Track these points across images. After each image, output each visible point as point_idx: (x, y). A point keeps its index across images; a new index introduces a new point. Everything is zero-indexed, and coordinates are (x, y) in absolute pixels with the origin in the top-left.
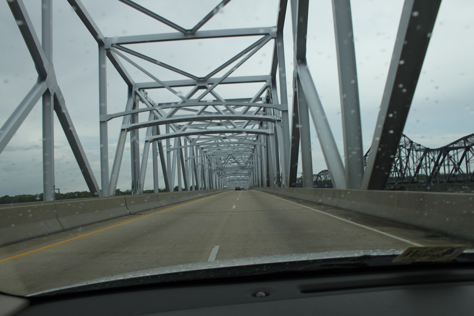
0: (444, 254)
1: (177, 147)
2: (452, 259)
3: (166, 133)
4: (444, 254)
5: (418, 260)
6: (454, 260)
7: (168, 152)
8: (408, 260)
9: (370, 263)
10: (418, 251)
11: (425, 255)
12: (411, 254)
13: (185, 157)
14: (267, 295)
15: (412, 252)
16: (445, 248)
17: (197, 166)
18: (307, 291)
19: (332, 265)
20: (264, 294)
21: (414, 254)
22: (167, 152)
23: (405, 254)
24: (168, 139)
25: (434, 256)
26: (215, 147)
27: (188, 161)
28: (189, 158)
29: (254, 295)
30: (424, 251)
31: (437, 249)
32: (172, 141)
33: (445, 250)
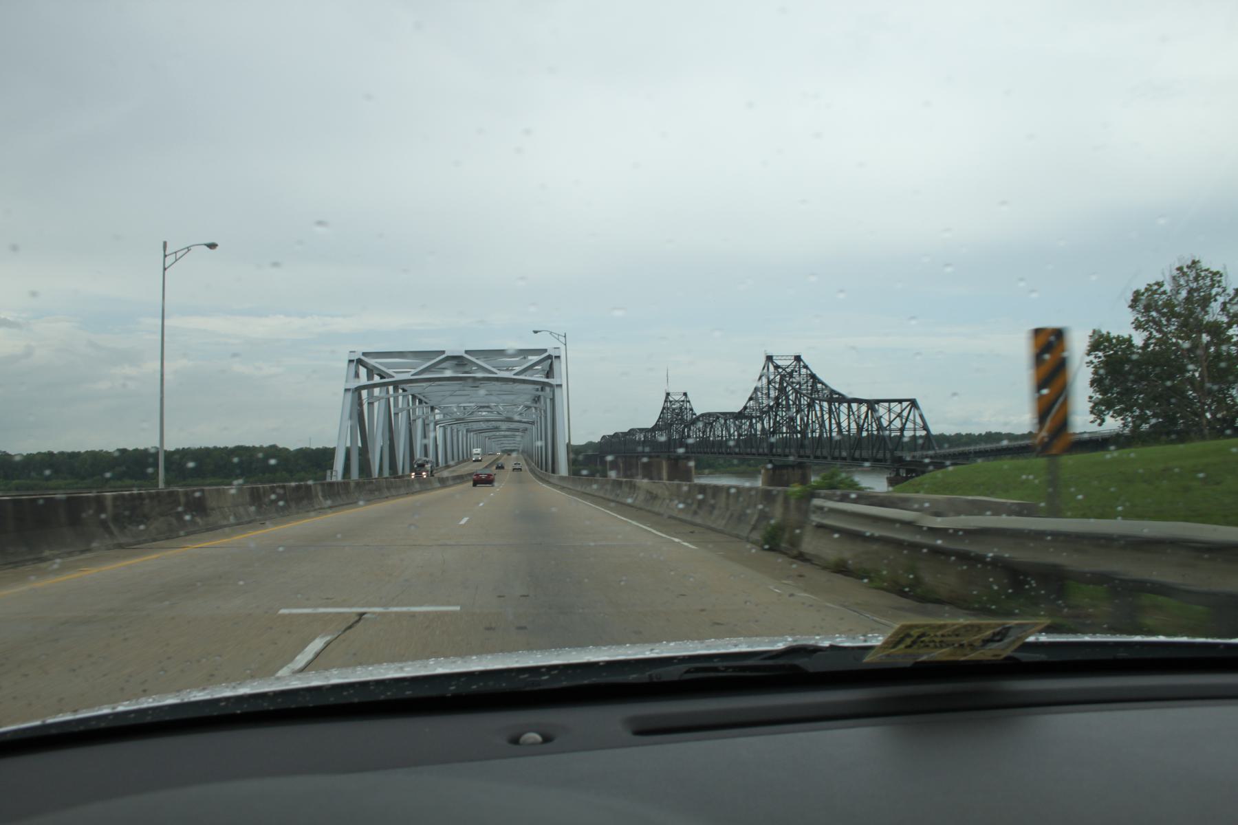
0: (986, 642)
1: (357, 478)
2: (1005, 654)
3: (368, 380)
4: (986, 642)
5: (924, 658)
6: (1008, 658)
7: (371, 404)
8: (903, 657)
9: (809, 665)
10: (923, 635)
11: (942, 644)
12: (908, 641)
13: (394, 406)
14: (547, 739)
15: (908, 635)
16: (988, 626)
17: (415, 420)
18: (647, 730)
19: (716, 669)
20: (538, 738)
21: (914, 643)
22: (368, 403)
23: (893, 642)
24: (371, 390)
25: (962, 645)
26: (379, 405)
27: (400, 414)
28: (402, 410)
29: (515, 741)
30: (939, 633)
31: (969, 629)
32: (377, 391)
33: (989, 633)
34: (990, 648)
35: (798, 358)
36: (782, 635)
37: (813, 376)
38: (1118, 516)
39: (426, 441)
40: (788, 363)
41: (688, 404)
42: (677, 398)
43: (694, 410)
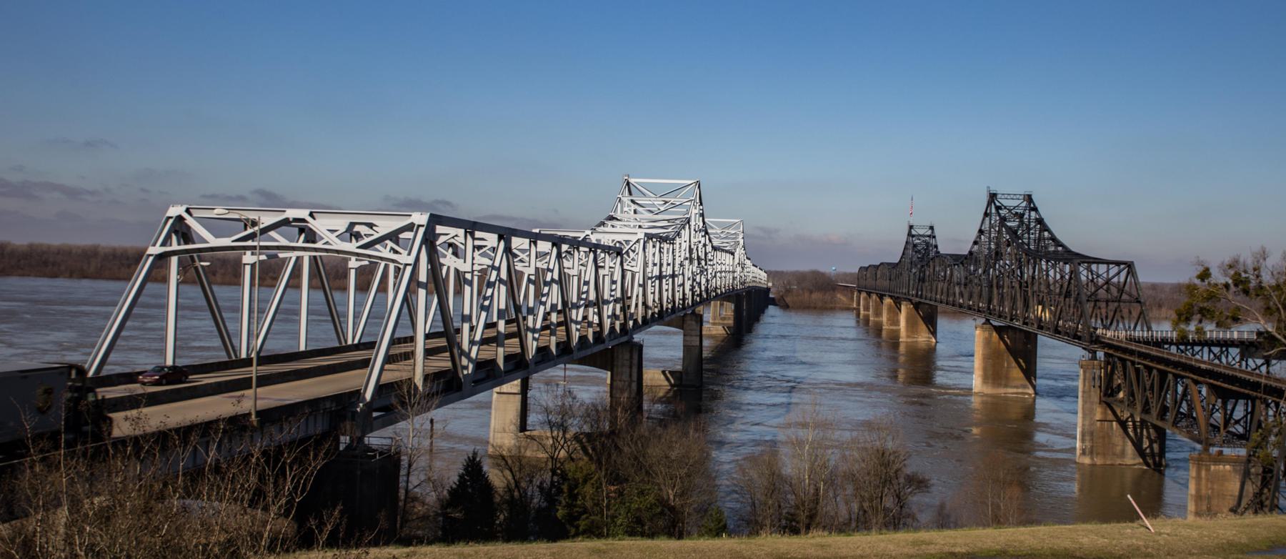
3: (303, 257)
34: (1101, 540)
35: (1029, 198)
36: (455, 518)
37: (1040, 221)
38: (1179, 367)
39: (618, 227)
40: (1015, 203)
41: (1033, 214)
42: (921, 232)
43: (939, 248)
